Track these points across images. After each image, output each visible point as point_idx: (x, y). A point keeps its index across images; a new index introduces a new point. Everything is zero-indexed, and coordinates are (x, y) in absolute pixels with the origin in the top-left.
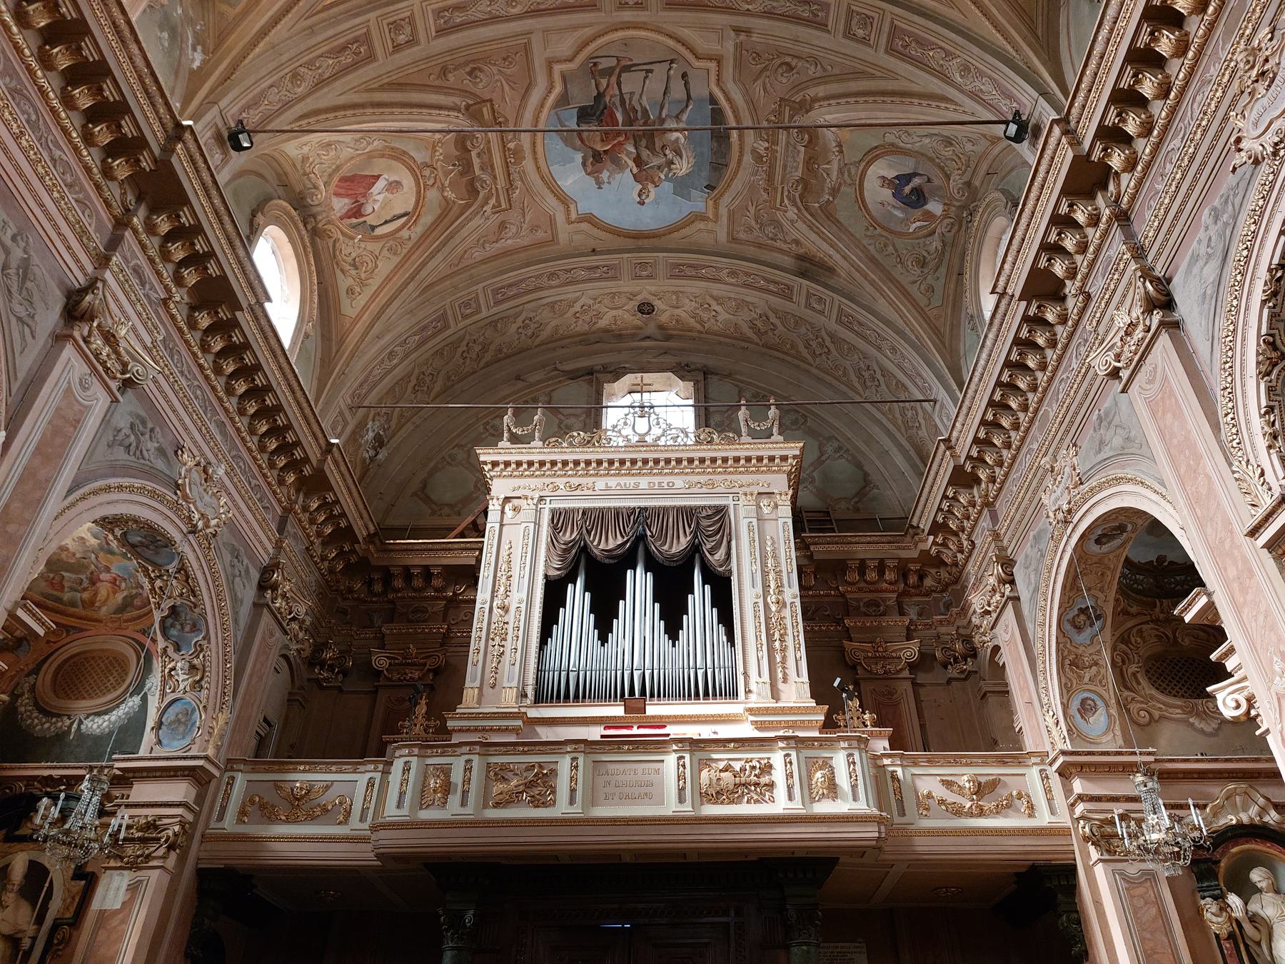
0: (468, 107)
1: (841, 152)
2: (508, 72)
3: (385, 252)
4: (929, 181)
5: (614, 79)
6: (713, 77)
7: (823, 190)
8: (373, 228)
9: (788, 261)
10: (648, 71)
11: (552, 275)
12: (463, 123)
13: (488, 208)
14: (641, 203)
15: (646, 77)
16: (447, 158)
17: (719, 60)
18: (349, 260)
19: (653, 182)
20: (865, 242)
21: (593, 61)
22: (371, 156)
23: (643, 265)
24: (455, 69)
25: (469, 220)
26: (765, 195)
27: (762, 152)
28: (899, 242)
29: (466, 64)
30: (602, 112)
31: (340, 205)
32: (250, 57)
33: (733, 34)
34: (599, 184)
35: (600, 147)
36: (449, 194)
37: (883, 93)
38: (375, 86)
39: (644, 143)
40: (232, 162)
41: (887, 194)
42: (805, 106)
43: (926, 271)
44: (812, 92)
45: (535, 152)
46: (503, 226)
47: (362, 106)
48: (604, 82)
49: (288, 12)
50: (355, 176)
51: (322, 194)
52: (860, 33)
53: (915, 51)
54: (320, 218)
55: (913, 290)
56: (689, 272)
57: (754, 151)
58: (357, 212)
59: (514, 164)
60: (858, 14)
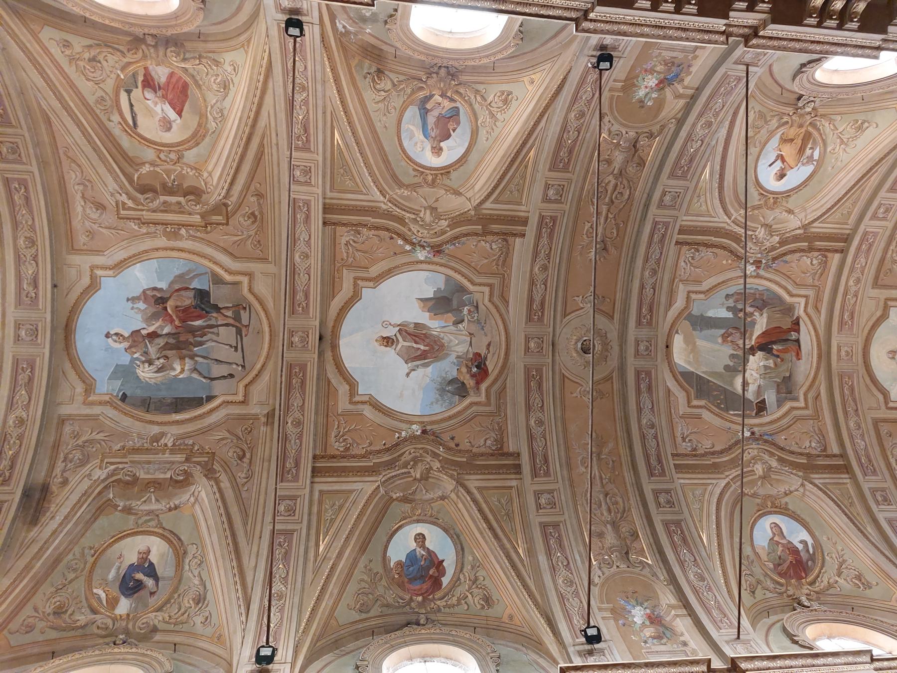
0: (226, 205)
1: (170, 510)
3: (100, 93)
4: (152, 594)
5: (231, 321)
7: (128, 500)
8: (129, 92)
9: (40, 476)
10: (236, 348)
11: (32, 242)
12: (214, 198)
13: (124, 198)
14: (108, 335)
15: (231, 346)
18: (101, 58)
19: (130, 347)
20: (77, 550)
21: (248, 307)
22: (202, 116)
23: (35, 332)
24: (259, 204)
25: (116, 178)
26: (118, 447)
27: (162, 441)
28: (80, 584)
29: (261, 213)
30: (203, 309)
31: (161, 74)
33: (266, 412)
34: (133, 300)
35: (170, 305)
36: (146, 169)
39: (172, 341)
40: (274, 10)
41: (132, 558)
42: (209, 473)
43: (51, 618)
44: (223, 478)
45: (172, 249)
46: (100, 207)
47: (254, 126)
48: (229, 313)
50: (186, 96)
51: (176, 63)
52: (282, 508)
53: (278, 553)
55: (28, 610)
56: (22, 378)
57: (163, 434)
58: (149, 83)
59: (165, 230)
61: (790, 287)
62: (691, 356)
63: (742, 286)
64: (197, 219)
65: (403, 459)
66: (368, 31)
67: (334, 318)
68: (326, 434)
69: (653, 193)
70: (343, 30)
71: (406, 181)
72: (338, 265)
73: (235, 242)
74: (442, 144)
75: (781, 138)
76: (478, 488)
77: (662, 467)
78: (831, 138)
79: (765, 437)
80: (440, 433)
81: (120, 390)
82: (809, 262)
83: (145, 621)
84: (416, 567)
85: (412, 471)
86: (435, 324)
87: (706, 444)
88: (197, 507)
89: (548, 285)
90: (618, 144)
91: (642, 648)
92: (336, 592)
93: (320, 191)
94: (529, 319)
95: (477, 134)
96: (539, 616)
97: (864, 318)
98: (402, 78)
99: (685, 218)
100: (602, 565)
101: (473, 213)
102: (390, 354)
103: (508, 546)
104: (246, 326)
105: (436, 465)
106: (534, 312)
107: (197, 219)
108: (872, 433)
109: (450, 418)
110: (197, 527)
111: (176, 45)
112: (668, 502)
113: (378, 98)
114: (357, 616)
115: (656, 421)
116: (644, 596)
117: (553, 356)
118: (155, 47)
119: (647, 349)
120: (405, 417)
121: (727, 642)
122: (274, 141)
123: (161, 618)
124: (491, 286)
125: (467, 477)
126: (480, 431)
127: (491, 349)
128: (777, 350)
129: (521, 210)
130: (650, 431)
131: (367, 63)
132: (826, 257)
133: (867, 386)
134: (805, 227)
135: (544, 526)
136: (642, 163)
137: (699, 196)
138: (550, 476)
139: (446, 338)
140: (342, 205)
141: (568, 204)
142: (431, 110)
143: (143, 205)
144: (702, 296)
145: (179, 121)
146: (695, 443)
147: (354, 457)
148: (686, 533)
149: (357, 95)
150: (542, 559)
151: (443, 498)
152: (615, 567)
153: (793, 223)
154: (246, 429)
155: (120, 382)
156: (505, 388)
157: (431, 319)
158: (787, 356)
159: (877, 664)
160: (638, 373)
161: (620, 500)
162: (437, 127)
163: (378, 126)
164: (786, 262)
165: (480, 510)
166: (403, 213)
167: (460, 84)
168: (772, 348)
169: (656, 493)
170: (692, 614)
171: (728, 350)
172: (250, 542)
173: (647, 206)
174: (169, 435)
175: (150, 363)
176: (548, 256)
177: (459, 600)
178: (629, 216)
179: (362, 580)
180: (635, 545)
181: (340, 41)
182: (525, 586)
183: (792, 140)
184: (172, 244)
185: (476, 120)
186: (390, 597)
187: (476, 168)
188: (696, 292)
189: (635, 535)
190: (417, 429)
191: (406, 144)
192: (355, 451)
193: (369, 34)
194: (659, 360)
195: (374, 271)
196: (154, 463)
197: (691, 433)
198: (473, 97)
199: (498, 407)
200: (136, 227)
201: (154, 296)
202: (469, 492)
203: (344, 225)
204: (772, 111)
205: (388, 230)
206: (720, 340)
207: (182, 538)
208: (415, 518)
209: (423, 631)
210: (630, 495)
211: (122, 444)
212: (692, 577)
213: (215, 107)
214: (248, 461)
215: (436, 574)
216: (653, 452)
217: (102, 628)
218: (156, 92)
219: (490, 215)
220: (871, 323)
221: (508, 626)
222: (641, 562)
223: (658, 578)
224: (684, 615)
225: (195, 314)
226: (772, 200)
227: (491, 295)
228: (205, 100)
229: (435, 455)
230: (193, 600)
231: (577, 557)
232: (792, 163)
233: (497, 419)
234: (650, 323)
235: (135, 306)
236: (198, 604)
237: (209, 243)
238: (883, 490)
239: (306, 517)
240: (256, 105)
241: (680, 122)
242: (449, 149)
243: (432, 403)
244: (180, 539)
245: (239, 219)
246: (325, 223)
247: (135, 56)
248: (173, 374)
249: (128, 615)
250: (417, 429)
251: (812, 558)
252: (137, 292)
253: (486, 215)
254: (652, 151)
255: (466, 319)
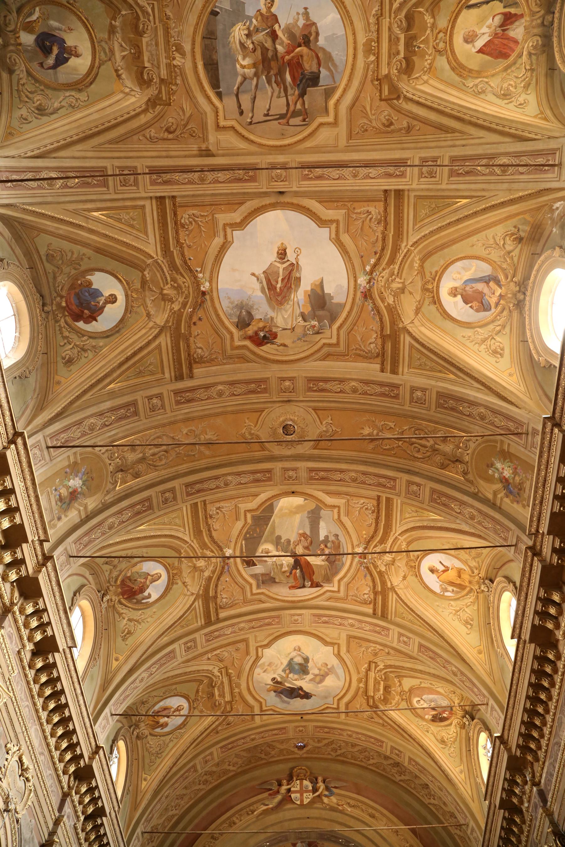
0: (398, 98)
1: (117, 71)
2: (365, 121)
4: (41, 65)
5: (292, 108)
6: (221, 114)
7: (122, 29)
10: (267, 115)
12: (405, 87)
15: (269, 110)
16: (423, 55)
17: (218, 127)
19: (262, 14)
21: (306, 122)
22: (479, 74)
24: (401, 129)
26: (168, 13)
27: (177, 55)
30: (301, 81)
31: (517, 31)
32: (526, 193)
34: (306, 14)
35: (303, 49)
36: (429, 19)
37: (99, 133)
38: (457, 134)
39: (270, 54)
41: (70, 41)
42: (152, 103)
44: (149, 116)
45: (355, 49)
47: (471, 123)
48: (299, 106)
49: (493, 206)
50: (496, 57)
54: (539, 21)
57: (183, 54)
58: (508, 19)
59: (372, 40)
60: (131, 185)
61: (345, 580)
62: (286, 511)
63: (346, 552)
64: (384, 71)
65: (178, 277)
66: (554, 230)
67: (301, 203)
68: (195, 206)
69: (420, 477)
70: (554, 208)
71: (427, 264)
72: (349, 204)
73: (364, 108)
74: (459, 297)
75: (461, 569)
76: (160, 345)
77: (194, 493)
78: (460, 603)
79: (226, 567)
80: (204, 308)
81: (221, 8)
82: (365, 592)
83: (17, 61)
84: (89, 298)
85: (169, 286)
86: (300, 296)
87: (216, 525)
88: (121, 95)
89: (340, 395)
90: (459, 447)
91: (51, 488)
92: (61, 232)
93: (414, 186)
94: (310, 380)
95: (468, 328)
96: (63, 406)
97: (324, 631)
98: (516, 259)
99: (399, 501)
100: (110, 452)
101: (401, 326)
102: (271, 257)
103: (115, 375)
104: (288, 122)
105: (176, 307)
106: (316, 383)
107: (384, 71)
108: (238, 638)
109: (218, 316)
110: (103, 98)
111: (544, 45)
112: (166, 500)
113: (497, 239)
114: (43, 252)
115: (231, 487)
116: (91, 485)
117: (279, 401)
118: (543, 24)
119: (290, 477)
120: (215, 275)
121: (66, 549)
122: (458, 143)
123: (21, 76)
124: (338, 344)
125: (168, 335)
126: (209, 343)
127: (281, 347)
128: (295, 573)
129: (404, 368)
130: (222, 483)
131: (528, 228)
132: (370, 603)
133: (273, 634)
134: (393, 589)
135: (134, 404)
136: (443, 467)
137: (417, 511)
138: (176, 405)
139: (288, 306)
140: (403, 206)
141: (410, 409)
142: (488, 286)
143: (394, 19)
144: (336, 517)
145: (474, 50)
146: (217, 517)
147: (177, 232)
148: (144, 514)
149: (500, 220)
150: (108, 405)
151: (148, 315)
152: (110, 462)
153: (395, 580)
154: (194, 132)
155: (228, 8)
156: (248, 362)
157: (305, 292)
158: (291, 580)
159: (67, 651)
160: (269, 471)
161: (163, 462)
162: (474, 292)
163: (474, 239)
164: (365, 576)
165: (141, 349)
166: (399, 263)
167: (510, 311)
168: (297, 569)
169: (173, 490)
170: (83, 522)
171: (293, 538)
172: (95, 148)
173: (409, 472)
174: (183, 61)
175: (248, 36)
176: (365, 393)
177: (67, 337)
178: (400, 458)
179: (73, 253)
180: (129, 476)
181: (543, 206)
182: (85, 392)
183: (460, 577)
184: (360, 48)
185: (480, 327)
186: (62, 279)
187: (439, 328)
188: (339, 512)
189: (137, 475)
190: (205, 287)
191: (459, 264)
192: (182, 233)
193: (552, 231)
194: (281, 487)
195: (346, 238)
196: (157, 50)
197: (224, 514)
198: (499, 323)
199: (231, 357)
200: (374, 12)
201: (310, 33)
202: (156, 337)
203: (386, 209)
204: (483, 562)
205: (383, 249)
206: (301, 532)
207: (92, 86)
208: (129, 293)
209: (38, 310)
210: (169, 470)
211: (172, 17)
212: (111, 520)
213: (487, 86)
214: (165, 137)
215: (85, 316)
216: (205, 486)
217: (5, 20)
218: (500, 27)
219: (399, 341)
220: (320, 634)
221: (52, 381)
222: (116, 482)
223: (106, 495)
224: (80, 516)
225: (296, 74)
226: (413, 564)
227: (330, 345)
228: (493, 76)
229: (184, 305)
230: (40, 104)
231: (113, 433)
232: (441, 578)
233: (220, 357)
234: (311, 478)
235: (300, 16)
236: (38, 109)
237: (363, 84)
238: (196, 647)
239: (120, 196)
240: (489, 125)
241: (475, 496)
242: (455, 303)
243: (229, 298)
244: (91, 83)
245: (386, 111)
246: (386, 191)
247: (534, 4)
248: (240, 58)
249: (20, 44)
250: (205, 287)
251: (139, 602)
252: (314, 17)
253: (399, 338)
254: (453, 474)
255: (306, 324)
